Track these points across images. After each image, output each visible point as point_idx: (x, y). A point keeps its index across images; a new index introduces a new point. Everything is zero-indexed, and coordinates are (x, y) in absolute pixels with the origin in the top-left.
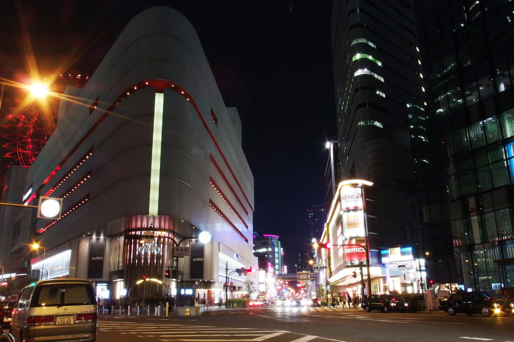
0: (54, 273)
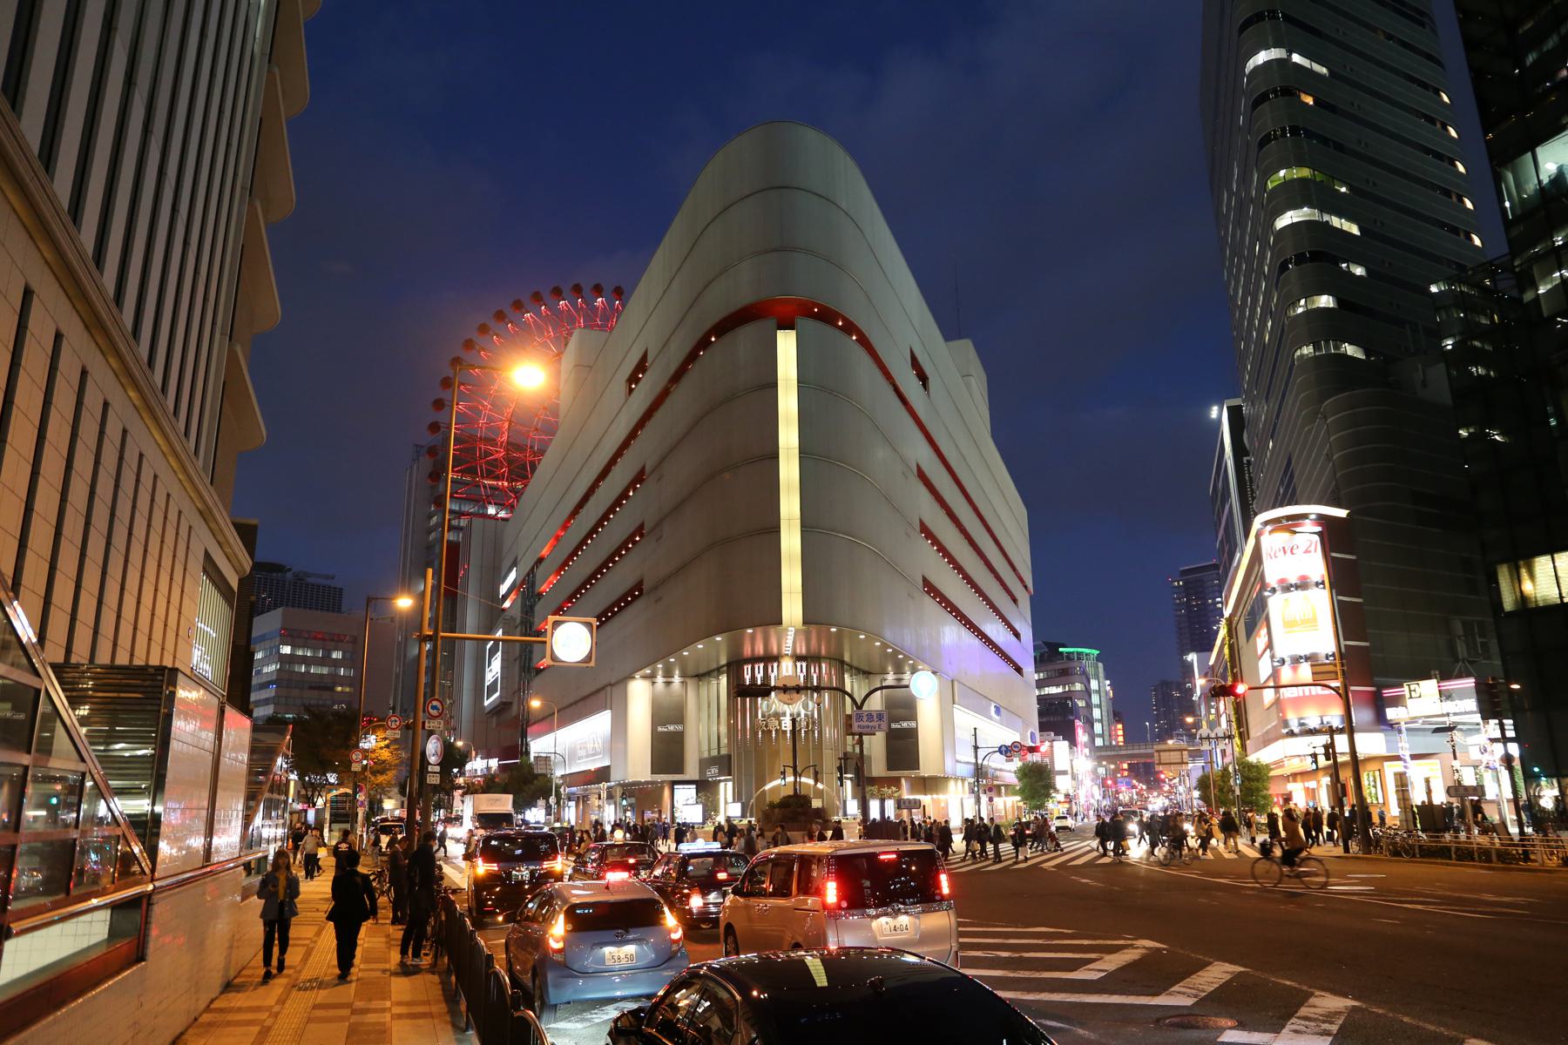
0: (578, 762)
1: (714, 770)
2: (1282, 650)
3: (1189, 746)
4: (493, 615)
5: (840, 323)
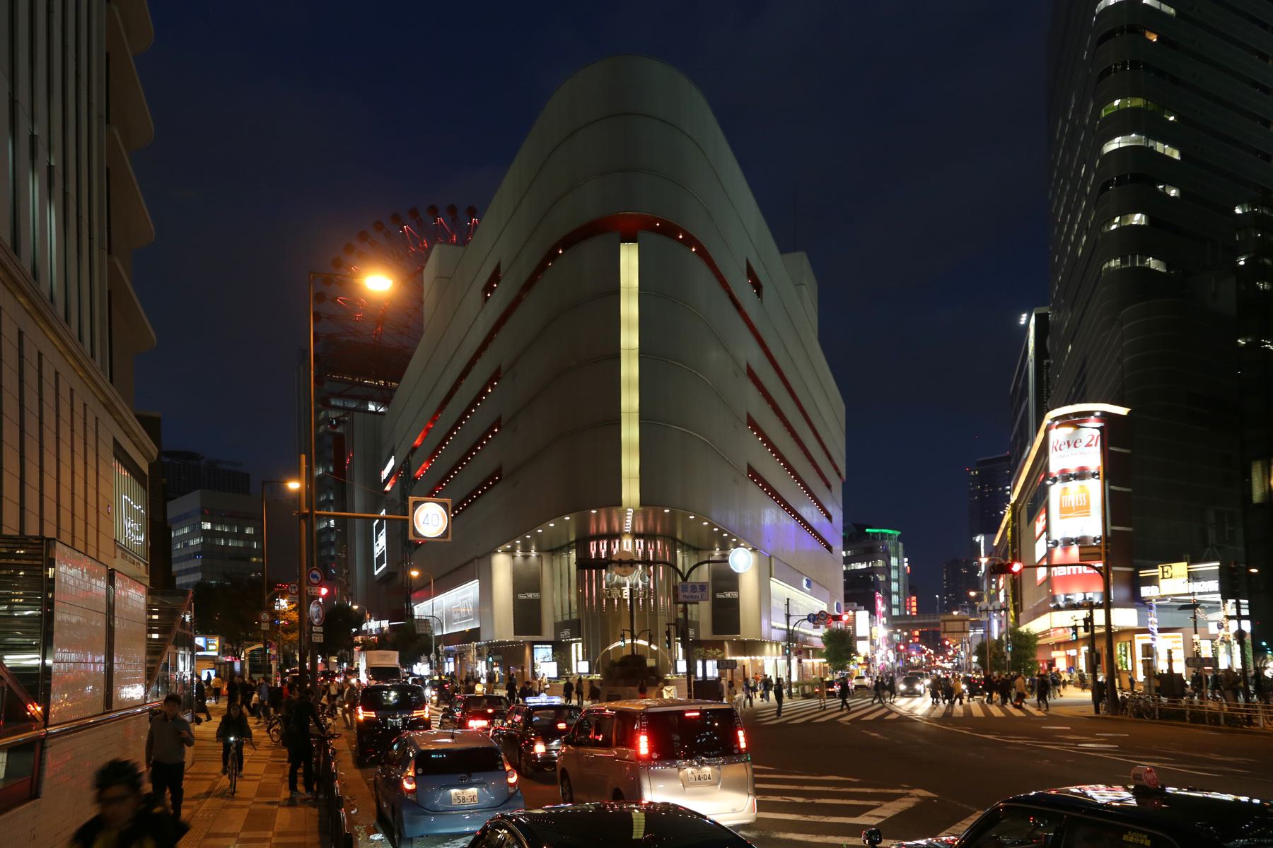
1: (567, 632)
2: (1057, 534)
3: (972, 617)
4: (377, 498)
5: (681, 237)
